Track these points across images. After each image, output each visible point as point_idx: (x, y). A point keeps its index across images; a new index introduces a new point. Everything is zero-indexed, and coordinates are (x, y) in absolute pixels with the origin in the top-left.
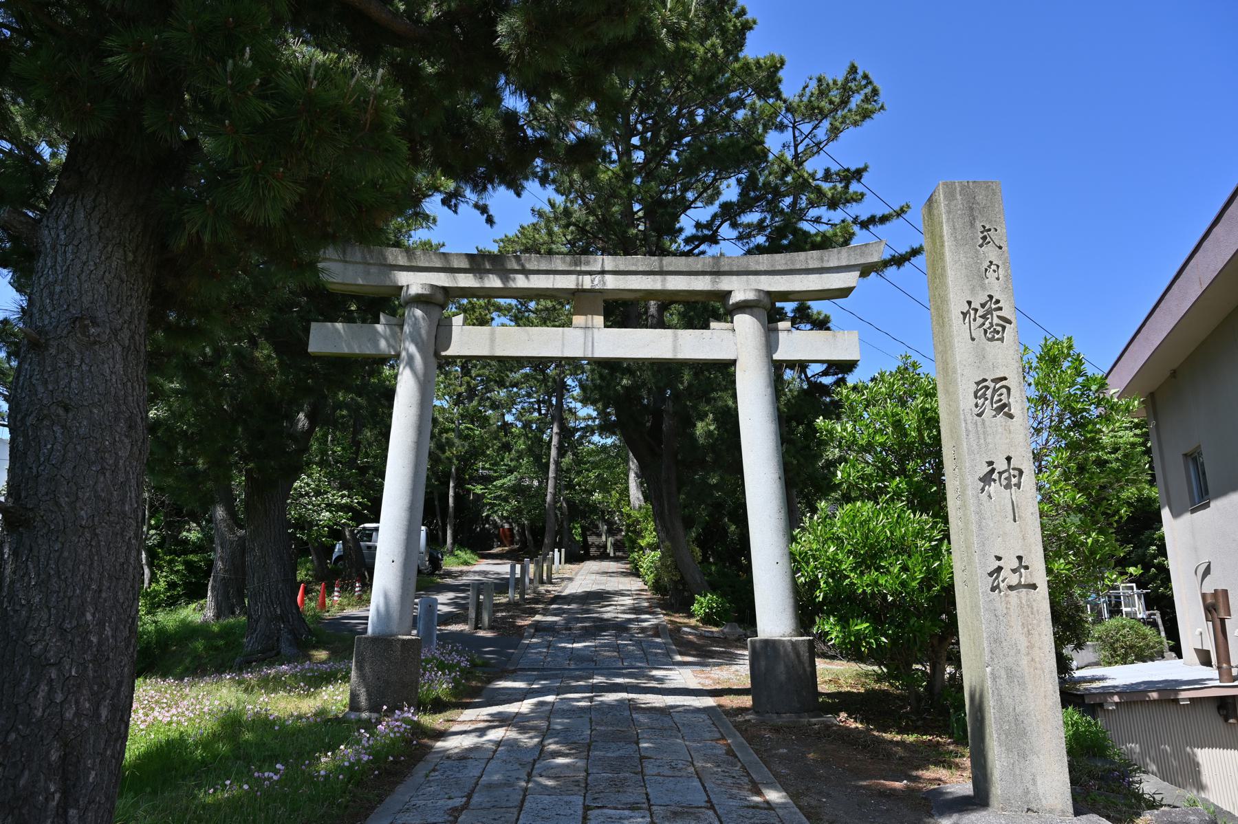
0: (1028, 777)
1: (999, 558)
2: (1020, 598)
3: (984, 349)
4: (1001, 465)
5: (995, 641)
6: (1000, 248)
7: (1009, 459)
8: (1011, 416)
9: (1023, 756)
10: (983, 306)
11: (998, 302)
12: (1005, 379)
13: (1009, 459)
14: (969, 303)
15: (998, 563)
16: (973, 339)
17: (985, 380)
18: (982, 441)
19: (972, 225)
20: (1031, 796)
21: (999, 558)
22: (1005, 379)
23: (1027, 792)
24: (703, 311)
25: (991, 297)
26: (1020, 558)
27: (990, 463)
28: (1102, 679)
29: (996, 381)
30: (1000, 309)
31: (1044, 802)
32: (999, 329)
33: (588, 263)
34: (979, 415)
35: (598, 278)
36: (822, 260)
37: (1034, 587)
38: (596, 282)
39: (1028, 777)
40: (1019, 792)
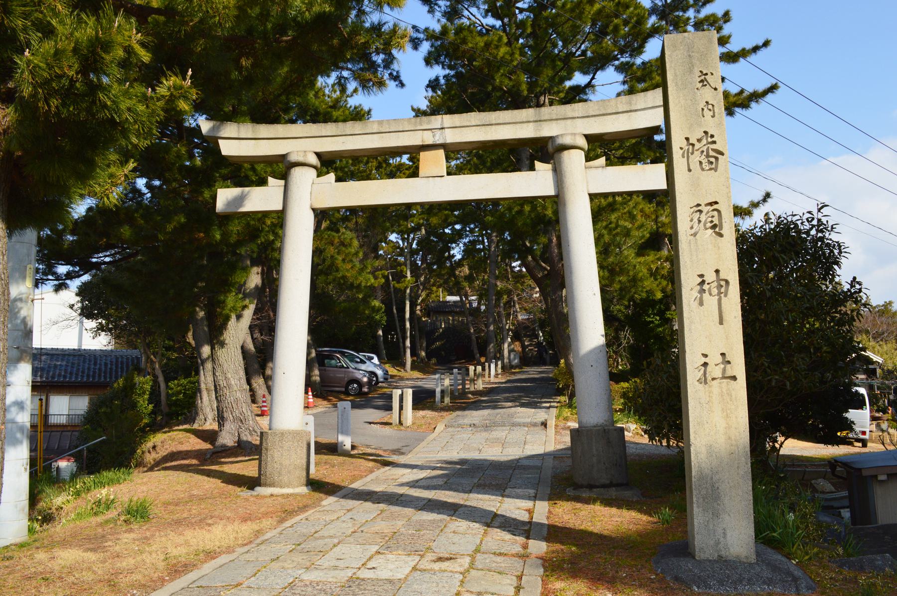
0: (720, 531)
1: (705, 356)
2: (721, 388)
3: (699, 178)
4: (710, 277)
5: (698, 423)
6: (716, 89)
7: (717, 271)
8: (721, 235)
9: (716, 515)
10: (699, 140)
11: (712, 136)
12: (716, 203)
13: (717, 271)
14: (687, 139)
15: (704, 360)
16: (690, 170)
17: (699, 205)
18: (694, 258)
19: (691, 71)
20: (721, 546)
21: (705, 356)
22: (716, 203)
23: (718, 543)
24: (543, 151)
25: (706, 133)
26: (723, 354)
27: (701, 276)
28: (381, 456)
29: (711, 204)
30: (714, 142)
31: (732, 550)
32: (713, 160)
33: (429, 123)
34: (695, 235)
35: (438, 133)
36: (630, 103)
37: (734, 378)
38: (437, 138)
39: (720, 531)
40: (712, 542)
